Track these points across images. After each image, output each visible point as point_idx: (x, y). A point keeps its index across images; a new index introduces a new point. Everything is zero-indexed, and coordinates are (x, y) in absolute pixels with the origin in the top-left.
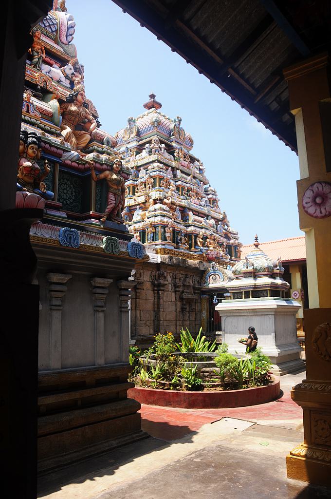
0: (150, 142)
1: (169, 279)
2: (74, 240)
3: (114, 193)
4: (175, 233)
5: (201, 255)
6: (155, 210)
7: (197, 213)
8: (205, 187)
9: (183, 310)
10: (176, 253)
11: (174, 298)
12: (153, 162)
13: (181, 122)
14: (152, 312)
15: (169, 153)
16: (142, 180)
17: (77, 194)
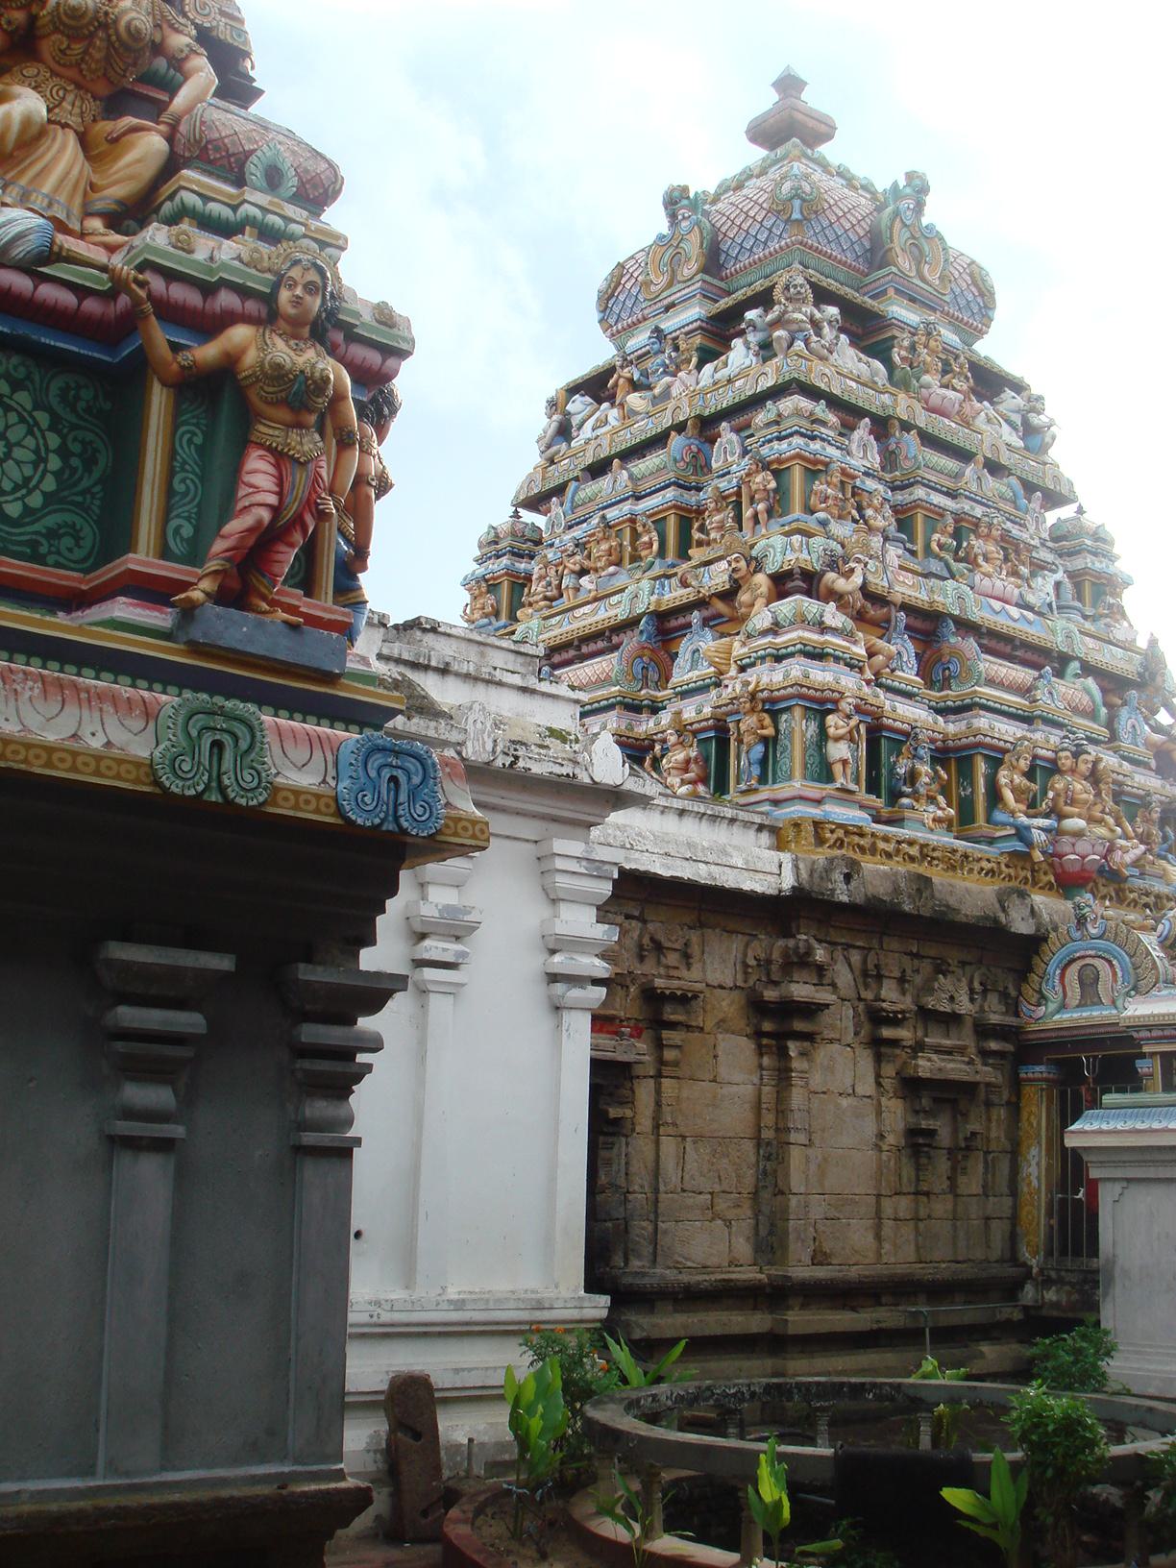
0: (764, 299)
1: (844, 976)
2: (413, 795)
3: (269, 449)
4: (878, 736)
5: (1021, 858)
6: (775, 629)
7: (1001, 644)
8: (1052, 517)
9: (918, 1142)
10: (881, 845)
11: (871, 1079)
12: (777, 392)
13: (929, 199)
14: (749, 1146)
15: (863, 350)
16: (723, 484)
17: (75, 462)
